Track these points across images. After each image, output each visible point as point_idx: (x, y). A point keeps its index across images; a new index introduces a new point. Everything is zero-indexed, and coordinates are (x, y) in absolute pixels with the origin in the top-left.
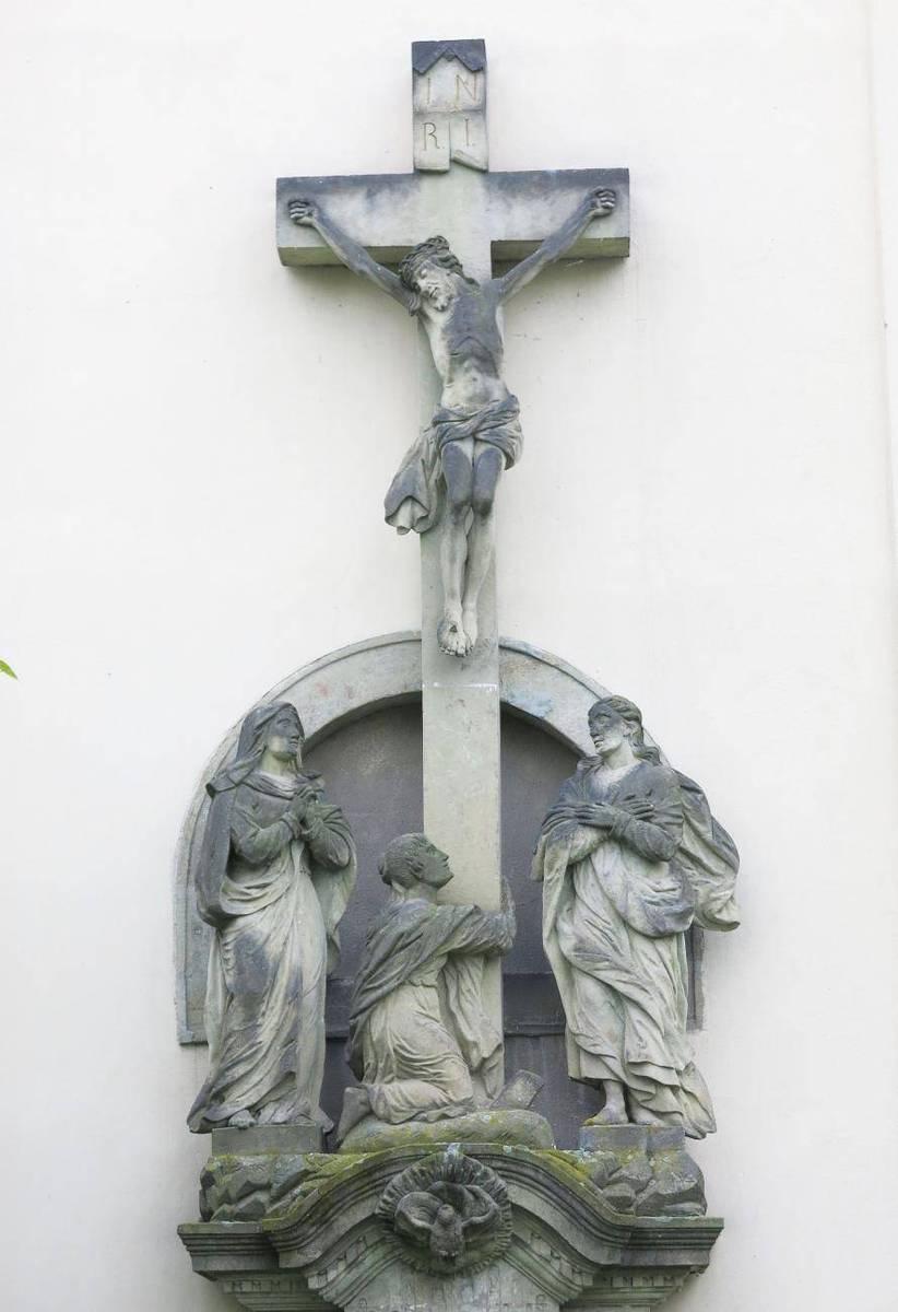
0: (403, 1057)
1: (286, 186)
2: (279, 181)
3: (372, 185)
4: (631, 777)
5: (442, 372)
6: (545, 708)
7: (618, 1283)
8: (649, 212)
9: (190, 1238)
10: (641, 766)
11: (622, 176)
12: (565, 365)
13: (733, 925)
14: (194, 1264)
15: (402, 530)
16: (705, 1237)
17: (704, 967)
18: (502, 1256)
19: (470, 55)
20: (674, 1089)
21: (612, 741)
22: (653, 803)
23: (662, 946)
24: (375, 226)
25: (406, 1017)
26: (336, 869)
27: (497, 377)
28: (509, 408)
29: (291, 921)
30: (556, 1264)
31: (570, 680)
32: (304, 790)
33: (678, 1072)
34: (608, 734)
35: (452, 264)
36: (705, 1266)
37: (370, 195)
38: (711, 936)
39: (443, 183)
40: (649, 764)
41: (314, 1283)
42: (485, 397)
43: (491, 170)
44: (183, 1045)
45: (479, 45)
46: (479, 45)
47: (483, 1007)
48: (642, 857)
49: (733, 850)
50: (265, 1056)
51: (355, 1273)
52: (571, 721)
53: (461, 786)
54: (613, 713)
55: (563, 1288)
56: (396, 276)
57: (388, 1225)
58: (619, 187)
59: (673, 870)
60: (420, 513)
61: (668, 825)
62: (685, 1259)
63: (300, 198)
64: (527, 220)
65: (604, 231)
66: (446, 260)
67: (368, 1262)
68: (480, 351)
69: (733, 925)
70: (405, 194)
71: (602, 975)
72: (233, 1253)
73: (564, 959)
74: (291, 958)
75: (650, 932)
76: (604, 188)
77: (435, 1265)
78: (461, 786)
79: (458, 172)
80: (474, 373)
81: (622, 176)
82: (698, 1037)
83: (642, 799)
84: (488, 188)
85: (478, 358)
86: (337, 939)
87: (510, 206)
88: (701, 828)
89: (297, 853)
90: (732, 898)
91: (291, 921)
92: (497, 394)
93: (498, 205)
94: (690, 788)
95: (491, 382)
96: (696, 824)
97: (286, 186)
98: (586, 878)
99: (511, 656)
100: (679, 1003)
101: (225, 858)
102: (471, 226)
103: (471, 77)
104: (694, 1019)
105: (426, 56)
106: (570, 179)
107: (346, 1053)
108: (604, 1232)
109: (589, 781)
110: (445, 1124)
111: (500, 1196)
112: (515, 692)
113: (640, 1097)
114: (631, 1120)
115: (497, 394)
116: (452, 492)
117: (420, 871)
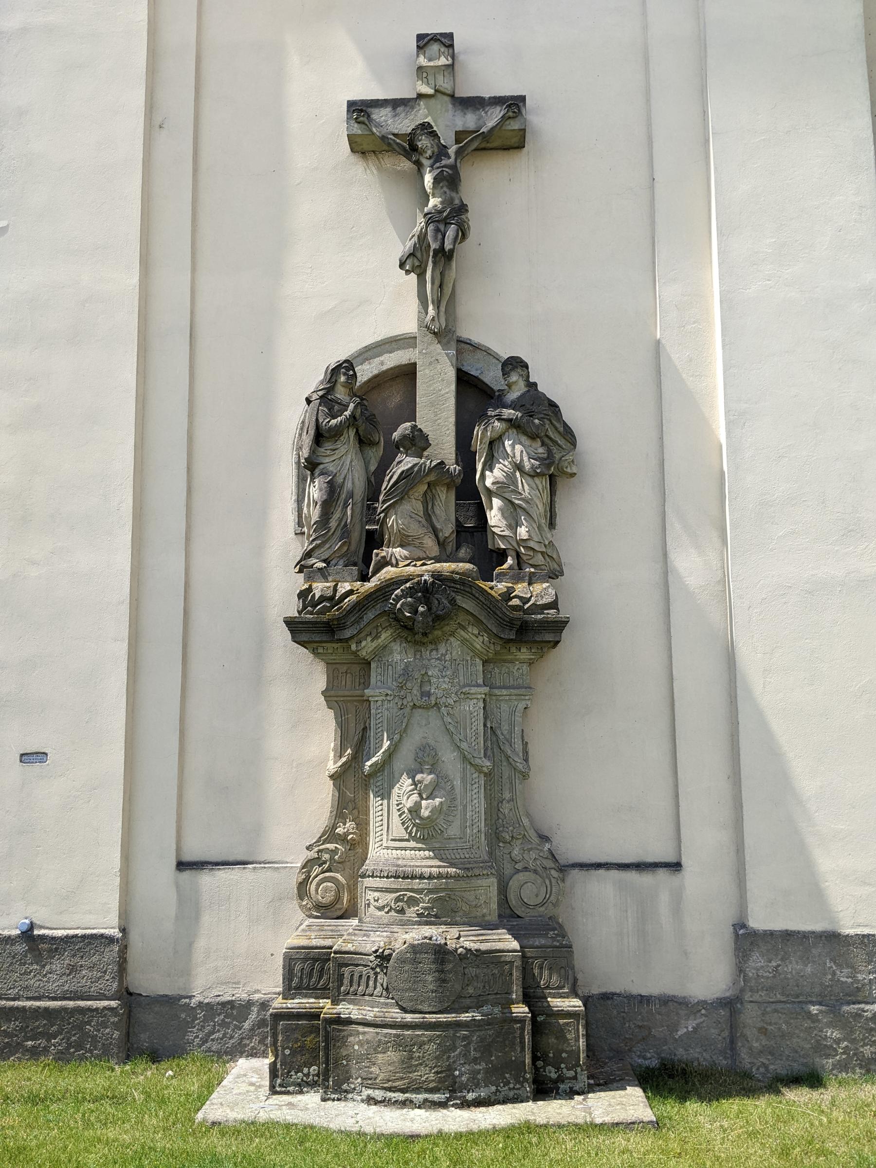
0: (404, 535)
1: (351, 104)
2: (348, 101)
3: (396, 104)
4: (523, 396)
5: (428, 191)
6: (479, 372)
7: (513, 650)
8: (538, 118)
9: (290, 623)
10: (528, 391)
11: (523, 99)
12: (491, 187)
13: (573, 475)
14: (293, 637)
15: (408, 272)
16: (559, 626)
17: (557, 499)
18: (453, 634)
19: (446, 41)
20: (542, 553)
21: (514, 377)
22: (534, 408)
23: (537, 481)
26: (373, 444)
27: (457, 193)
28: (463, 208)
30: (481, 638)
31: (491, 357)
32: (358, 411)
33: (545, 546)
34: (512, 373)
35: (434, 135)
36: (558, 642)
37: (394, 108)
38: (560, 483)
39: (432, 101)
40: (532, 390)
41: (354, 647)
42: (452, 200)
43: (456, 95)
44: (296, 534)
45: (450, 36)
46: (450, 36)
48: (418, 1136)
49: (574, 436)
50: (333, 534)
51: (374, 644)
52: (492, 377)
53: (436, 409)
54: (515, 365)
55: (485, 652)
56: (408, 147)
57: (395, 618)
58: (521, 104)
59: (543, 444)
60: (417, 263)
61: (540, 418)
62: (549, 637)
63: (360, 110)
64: (469, 121)
65: (515, 125)
66: (431, 132)
67: (383, 637)
68: (450, 180)
69: (573, 475)
70: (413, 108)
71: (507, 495)
72: (313, 632)
73: (488, 489)
74: (349, 485)
75: (532, 474)
76: (514, 105)
77: (418, 637)
79: (439, 95)
80: (445, 189)
81: (523, 99)
82: (554, 532)
83: (528, 406)
84: (454, 105)
85: (448, 181)
86: (373, 480)
87: (465, 114)
88: (558, 425)
89: (352, 433)
90: (573, 461)
92: (457, 202)
93: (459, 113)
94: (553, 405)
95: (454, 194)
96: (555, 423)
97: (351, 104)
98: (499, 448)
99: (463, 345)
100: (545, 511)
103: (446, 49)
104: (552, 525)
105: (424, 41)
106: (498, 101)
108: (510, 623)
109: (501, 400)
110: (424, 568)
111: (453, 602)
112: (465, 364)
113: (525, 558)
114: (520, 569)
115: (457, 202)
116: (437, 255)
117: (417, 442)
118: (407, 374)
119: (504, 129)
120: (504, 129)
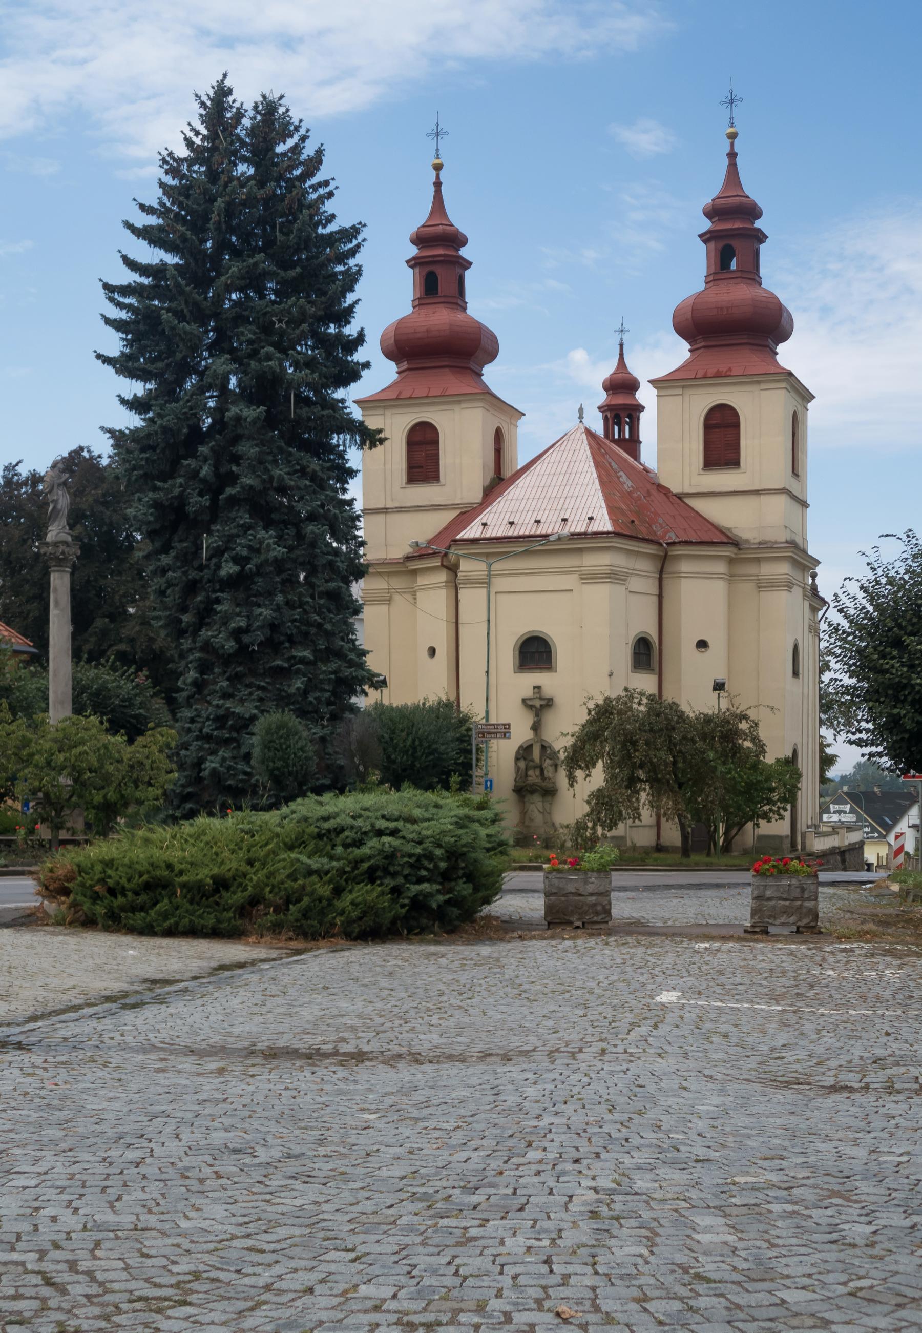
24: (530, 703)
25: (530, 773)
29: (522, 764)
32: (524, 752)
47: (538, 772)
63: (524, 700)
64: (543, 702)
78: (536, 751)
91: (522, 764)
101: (517, 759)
102: (538, 703)
107: (526, 775)
117: (533, 761)
118: (531, 746)
119: (549, 703)
120: (549, 703)
